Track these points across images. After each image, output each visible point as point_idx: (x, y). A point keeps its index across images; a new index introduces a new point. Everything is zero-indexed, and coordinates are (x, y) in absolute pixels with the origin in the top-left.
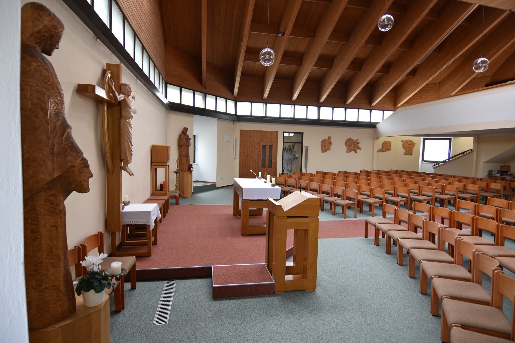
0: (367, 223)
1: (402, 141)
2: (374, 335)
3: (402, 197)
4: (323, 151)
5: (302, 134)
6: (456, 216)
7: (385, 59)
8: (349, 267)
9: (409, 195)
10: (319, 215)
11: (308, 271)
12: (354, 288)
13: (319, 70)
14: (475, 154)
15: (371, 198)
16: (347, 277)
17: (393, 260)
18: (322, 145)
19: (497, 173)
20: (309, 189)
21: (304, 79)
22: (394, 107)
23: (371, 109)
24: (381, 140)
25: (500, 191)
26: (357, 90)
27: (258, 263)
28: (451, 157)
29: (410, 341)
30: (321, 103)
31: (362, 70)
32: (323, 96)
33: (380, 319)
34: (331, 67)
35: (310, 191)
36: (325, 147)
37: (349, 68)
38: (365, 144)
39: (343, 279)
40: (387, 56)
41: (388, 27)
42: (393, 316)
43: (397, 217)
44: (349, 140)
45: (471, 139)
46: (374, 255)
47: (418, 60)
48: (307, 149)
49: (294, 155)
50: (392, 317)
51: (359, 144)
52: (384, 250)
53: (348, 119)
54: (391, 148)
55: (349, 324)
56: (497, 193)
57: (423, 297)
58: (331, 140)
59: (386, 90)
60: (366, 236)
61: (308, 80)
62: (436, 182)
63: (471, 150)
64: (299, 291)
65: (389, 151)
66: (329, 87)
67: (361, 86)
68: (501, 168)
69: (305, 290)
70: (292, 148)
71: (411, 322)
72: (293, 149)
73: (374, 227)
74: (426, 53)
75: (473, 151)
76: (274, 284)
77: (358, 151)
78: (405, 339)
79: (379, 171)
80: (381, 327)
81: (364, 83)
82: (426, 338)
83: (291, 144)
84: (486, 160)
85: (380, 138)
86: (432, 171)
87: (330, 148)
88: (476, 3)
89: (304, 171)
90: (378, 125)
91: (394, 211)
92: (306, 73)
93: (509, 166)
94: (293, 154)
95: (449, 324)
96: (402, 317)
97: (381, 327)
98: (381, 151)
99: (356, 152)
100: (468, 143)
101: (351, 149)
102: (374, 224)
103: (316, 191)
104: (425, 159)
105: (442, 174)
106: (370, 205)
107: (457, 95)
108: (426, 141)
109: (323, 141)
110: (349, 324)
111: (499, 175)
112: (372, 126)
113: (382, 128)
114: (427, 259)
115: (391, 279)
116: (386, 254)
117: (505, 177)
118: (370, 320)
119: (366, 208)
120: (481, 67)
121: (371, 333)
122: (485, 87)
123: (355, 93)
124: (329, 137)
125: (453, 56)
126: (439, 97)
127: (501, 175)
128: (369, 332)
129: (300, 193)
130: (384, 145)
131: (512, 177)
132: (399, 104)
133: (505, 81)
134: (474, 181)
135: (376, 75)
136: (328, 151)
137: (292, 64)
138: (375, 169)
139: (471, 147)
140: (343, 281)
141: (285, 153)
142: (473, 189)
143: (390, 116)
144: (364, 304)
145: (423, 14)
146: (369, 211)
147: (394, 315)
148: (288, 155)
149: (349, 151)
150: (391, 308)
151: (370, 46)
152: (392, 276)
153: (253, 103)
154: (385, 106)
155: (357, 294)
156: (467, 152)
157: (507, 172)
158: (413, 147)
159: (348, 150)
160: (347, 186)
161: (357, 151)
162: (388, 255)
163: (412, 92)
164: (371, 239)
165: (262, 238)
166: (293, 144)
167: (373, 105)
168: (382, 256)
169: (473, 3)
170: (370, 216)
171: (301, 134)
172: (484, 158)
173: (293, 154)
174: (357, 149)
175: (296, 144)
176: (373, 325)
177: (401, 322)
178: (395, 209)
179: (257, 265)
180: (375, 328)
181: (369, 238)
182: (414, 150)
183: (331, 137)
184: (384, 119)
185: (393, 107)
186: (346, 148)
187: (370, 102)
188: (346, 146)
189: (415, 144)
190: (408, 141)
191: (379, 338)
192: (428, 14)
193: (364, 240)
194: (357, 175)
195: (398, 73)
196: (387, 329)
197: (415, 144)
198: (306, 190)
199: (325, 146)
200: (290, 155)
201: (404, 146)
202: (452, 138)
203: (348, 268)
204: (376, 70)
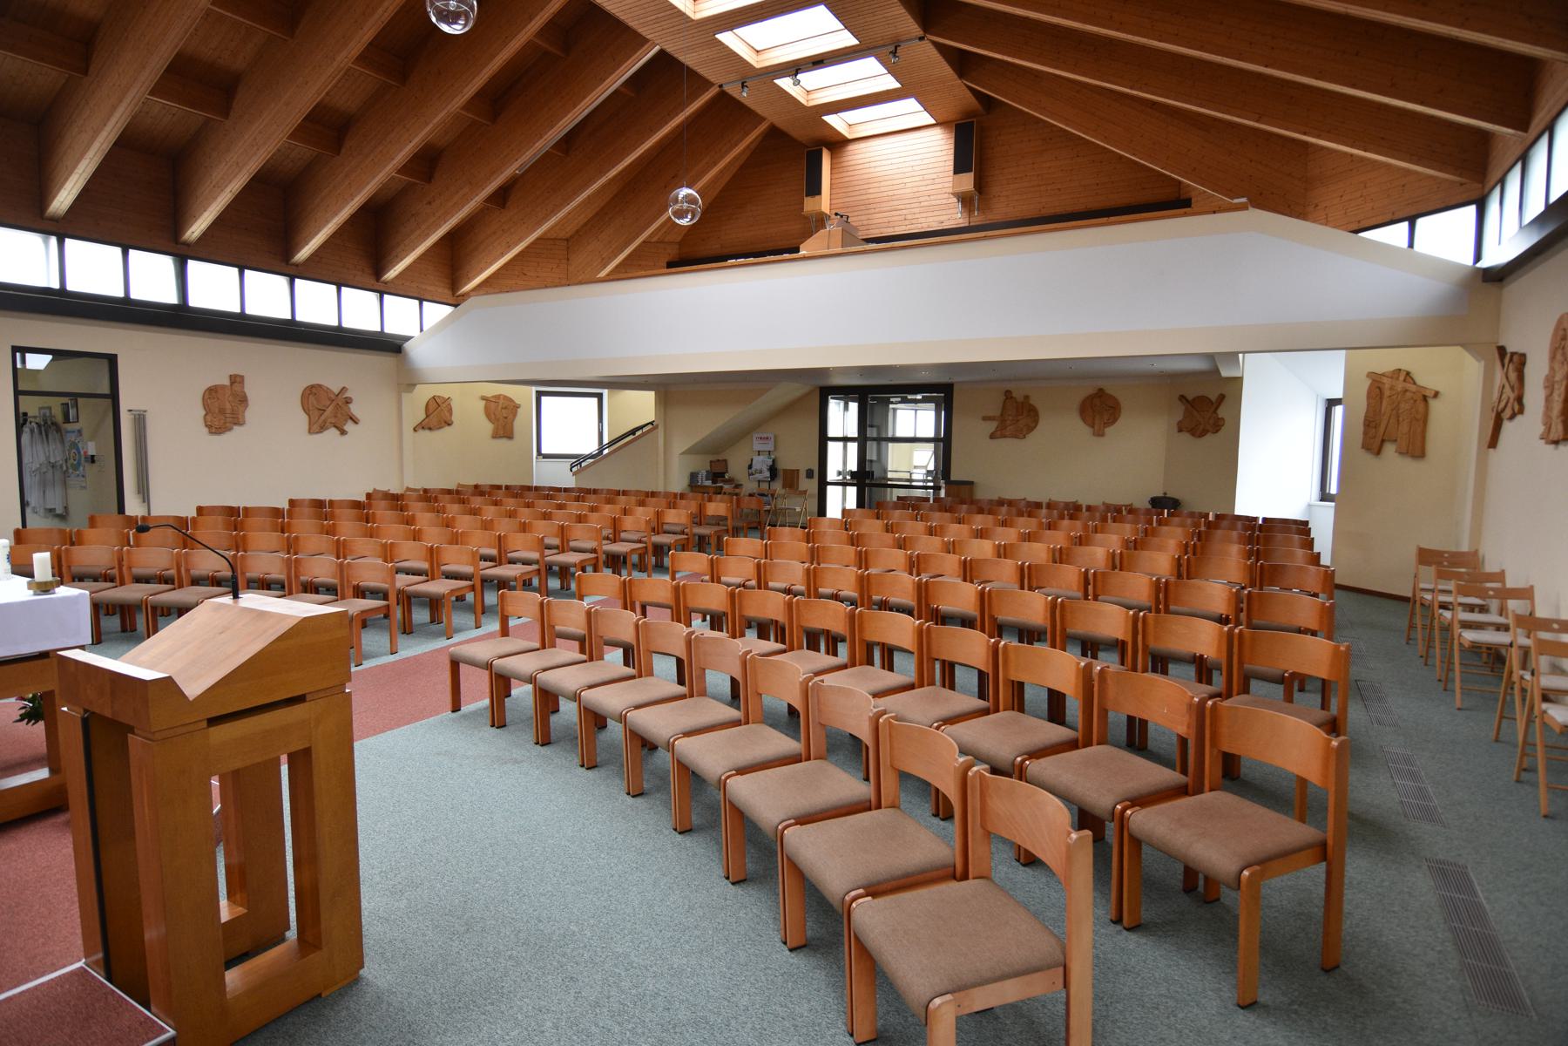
0: (455, 665)
1: (483, 398)
2: (628, 1033)
3: (523, 564)
4: (214, 430)
5: (112, 360)
6: (689, 596)
7: (423, 133)
8: (445, 829)
9: (543, 555)
10: (350, 680)
11: (324, 916)
12: (494, 900)
13: (171, 115)
14: (660, 432)
15: (433, 579)
16: (456, 871)
17: (566, 759)
18: (206, 406)
19: (707, 479)
20: (185, 581)
21: (104, 134)
22: (450, 293)
23: (382, 289)
24: (423, 394)
25: (725, 519)
26: (333, 217)
27: (43, 975)
28: (606, 441)
29: (723, 991)
30: (187, 244)
31: (343, 151)
32: (195, 218)
33: (616, 965)
34: (226, 112)
35: (305, 591)
36: (220, 411)
37: (299, 133)
38: (371, 404)
39: (444, 885)
40: (431, 126)
41: (460, 22)
42: (645, 939)
43: (549, 625)
44: (314, 390)
45: (649, 397)
46: (506, 763)
47: (517, 160)
48: (140, 420)
49: (74, 445)
50: (644, 941)
51: (350, 406)
52: (530, 736)
53: (78, 283)
54: (453, 419)
55: (536, 1039)
56: (718, 524)
57: (686, 841)
58: (246, 390)
59: (427, 236)
60: (456, 708)
61: (124, 143)
62: (528, 505)
63: (651, 423)
64: (294, 1010)
65: (447, 429)
66: (220, 187)
67: (344, 207)
68: (711, 466)
69: (319, 995)
70: (59, 418)
71: (696, 932)
72: (67, 420)
73: (487, 673)
74: (539, 144)
75: (657, 427)
76: (172, 1040)
77: (349, 426)
78: (708, 991)
79: (426, 491)
80: (634, 992)
81: (356, 199)
82: (752, 957)
83: (56, 404)
84: (683, 450)
85: (418, 386)
86: (568, 481)
87: (244, 416)
88: (657, 42)
89: (133, 507)
90: (407, 345)
91: (537, 609)
92: (114, 108)
93: (725, 461)
94: (67, 445)
95: (836, 904)
96: (669, 926)
97: (634, 992)
98: (423, 428)
99: (343, 432)
100: (642, 407)
101: (325, 422)
102: (486, 660)
103: (331, 589)
104: (544, 451)
105: (596, 488)
106: (434, 604)
107: (614, 277)
108: (543, 398)
109: (212, 393)
110: (536, 1039)
111: (709, 483)
112: (388, 345)
113: (422, 352)
114: (688, 729)
115: (587, 823)
116: (538, 747)
117: (721, 487)
118: (591, 987)
119: (421, 615)
120: (687, 212)
121: (617, 1029)
122: (668, 267)
123: (325, 226)
124: (236, 376)
125: (602, 172)
126: (569, 279)
127: (714, 482)
128: (609, 1030)
129: (236, 603)
130: (431, 412)
131: (733, 485)
132: (466, 284)
133: (724, 258)
134: (673, 500)
135: (393, 178)
136: (235, 427)
137: (42, 60)
138: (410, 486)
139: (651, 417)
140: (447, 892)
141: (25, 438)
142: (676, 521)
143: (442, 320)
144: (550, 940)
145: (532, 23)
146: (431, 622)
147: (645, 931)
148: (39, 447)
149: (317, 427)
150: (629, 915)
151: (371, 76)
152: (586, 810)
153: (297, 280)
154: (424, 287)
155: (512, 919)
156: (645, 430)
157: (722, 475)
158: (515, 415)
159: (315, 426)
160: (341, 550)
161: (346, 428)
162: (545, 748)
163: (502, 255)
164: (476, 714)
165: (13, 846)
166: (65, 400)
167: (386, 277)
168: (528, 758)
169: (648, 37)
170: (440, 639)
171: (105, 363)
172: (680, 444)
173: (67, 445)
174: (346, 421)
175: (80, 400)
176: (608, 998)
177: (675, 947)
178: (542, 604)
179: (42, 984)
180: (617, 1004)
181: (465, 709)
182: (518, 424)
183: (242, 377)
184: (425, 329)
185: (448, 292)
186: (305, 418)
187: (378, 269)
188: (306, 410)
189: (517, 407)
190: (498, 397)
191: (644, 1033)
192: (543, 32)
193: (454, 720)
194: (362, 509)
195: (461, 189)
196: (651, 987)
197: (518, 408)
198: (283, 587)
199: (222, 411)
200: (52, 447)
201: (489, 413)
202: (605, 392)
203: (444, 838)
204: (395, 162)
